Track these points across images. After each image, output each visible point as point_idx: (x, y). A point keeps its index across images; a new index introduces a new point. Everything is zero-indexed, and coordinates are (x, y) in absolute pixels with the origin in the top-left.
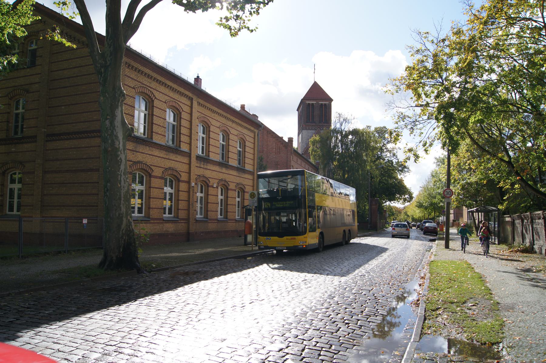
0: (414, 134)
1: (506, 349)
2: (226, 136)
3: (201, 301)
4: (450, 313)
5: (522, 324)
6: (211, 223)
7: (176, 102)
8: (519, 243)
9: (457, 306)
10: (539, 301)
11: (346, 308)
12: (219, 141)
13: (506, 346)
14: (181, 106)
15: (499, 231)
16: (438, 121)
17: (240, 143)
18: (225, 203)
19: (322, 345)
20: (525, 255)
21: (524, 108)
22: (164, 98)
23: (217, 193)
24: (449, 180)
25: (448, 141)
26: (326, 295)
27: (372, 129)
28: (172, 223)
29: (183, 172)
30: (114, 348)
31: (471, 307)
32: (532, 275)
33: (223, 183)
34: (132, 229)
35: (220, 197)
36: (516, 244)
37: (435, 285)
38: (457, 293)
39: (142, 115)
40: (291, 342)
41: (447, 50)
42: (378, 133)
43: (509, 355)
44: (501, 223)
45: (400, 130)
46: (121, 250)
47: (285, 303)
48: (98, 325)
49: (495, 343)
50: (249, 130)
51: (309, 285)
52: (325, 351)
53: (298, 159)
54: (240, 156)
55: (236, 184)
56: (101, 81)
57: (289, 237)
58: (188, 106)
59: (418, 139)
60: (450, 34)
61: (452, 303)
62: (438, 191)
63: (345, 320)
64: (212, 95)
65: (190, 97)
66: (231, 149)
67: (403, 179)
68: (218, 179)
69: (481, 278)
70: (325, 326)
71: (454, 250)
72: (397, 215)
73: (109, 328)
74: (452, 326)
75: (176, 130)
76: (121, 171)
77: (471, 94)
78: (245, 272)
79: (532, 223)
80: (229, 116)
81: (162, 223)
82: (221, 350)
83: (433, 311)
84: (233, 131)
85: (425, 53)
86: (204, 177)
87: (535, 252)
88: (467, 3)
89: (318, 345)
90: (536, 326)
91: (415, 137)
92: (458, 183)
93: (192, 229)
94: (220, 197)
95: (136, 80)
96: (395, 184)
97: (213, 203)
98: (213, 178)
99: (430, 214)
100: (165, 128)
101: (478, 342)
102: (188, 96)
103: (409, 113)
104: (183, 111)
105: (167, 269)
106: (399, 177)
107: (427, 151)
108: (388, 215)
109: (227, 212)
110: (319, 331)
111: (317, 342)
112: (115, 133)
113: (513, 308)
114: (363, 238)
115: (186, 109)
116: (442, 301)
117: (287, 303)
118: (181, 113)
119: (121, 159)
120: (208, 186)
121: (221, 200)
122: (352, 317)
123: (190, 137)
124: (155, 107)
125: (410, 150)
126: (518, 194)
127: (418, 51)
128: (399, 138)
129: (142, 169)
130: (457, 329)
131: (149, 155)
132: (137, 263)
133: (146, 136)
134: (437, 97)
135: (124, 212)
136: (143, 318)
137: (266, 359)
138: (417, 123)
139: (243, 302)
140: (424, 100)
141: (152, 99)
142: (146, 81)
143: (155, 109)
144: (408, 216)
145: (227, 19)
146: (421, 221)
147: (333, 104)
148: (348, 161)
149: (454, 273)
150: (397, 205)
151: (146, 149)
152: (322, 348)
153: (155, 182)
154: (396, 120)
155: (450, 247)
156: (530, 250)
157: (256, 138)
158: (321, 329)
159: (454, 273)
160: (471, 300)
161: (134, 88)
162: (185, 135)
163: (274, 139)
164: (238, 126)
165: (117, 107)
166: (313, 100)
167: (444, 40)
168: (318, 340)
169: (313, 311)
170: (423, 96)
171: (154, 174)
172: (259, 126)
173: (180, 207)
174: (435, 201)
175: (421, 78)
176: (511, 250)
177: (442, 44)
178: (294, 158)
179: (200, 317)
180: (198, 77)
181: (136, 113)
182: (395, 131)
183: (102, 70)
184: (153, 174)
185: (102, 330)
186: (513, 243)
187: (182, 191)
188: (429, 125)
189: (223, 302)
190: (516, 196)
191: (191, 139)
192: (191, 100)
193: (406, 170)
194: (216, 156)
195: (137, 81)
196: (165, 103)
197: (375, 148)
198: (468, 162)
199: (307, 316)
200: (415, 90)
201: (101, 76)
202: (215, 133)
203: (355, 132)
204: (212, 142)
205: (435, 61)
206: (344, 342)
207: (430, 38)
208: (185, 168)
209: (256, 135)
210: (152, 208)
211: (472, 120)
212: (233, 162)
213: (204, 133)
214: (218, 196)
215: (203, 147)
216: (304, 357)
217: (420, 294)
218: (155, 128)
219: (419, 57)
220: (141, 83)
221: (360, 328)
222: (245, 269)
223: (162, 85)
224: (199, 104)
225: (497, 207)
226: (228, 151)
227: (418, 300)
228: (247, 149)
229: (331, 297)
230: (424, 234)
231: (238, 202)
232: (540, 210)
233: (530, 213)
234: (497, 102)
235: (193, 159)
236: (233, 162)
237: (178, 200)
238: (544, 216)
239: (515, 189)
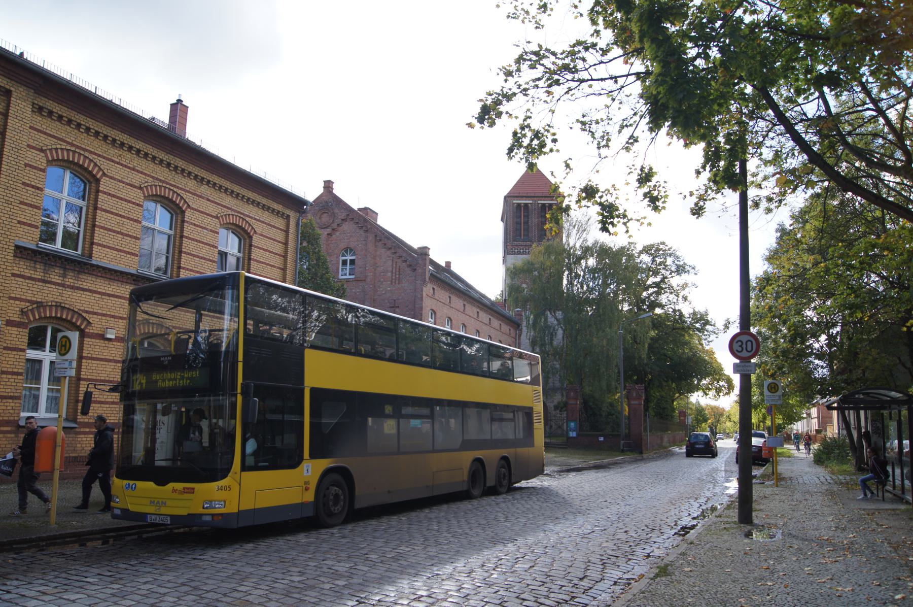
14: (185, 197)
53: (467, 305)
57: (179, 486)
64: (48, 67)
133: (79, 252)
161: (217, 217)
163: (389, 252)
166: (527, 197)
180: (179, 101)
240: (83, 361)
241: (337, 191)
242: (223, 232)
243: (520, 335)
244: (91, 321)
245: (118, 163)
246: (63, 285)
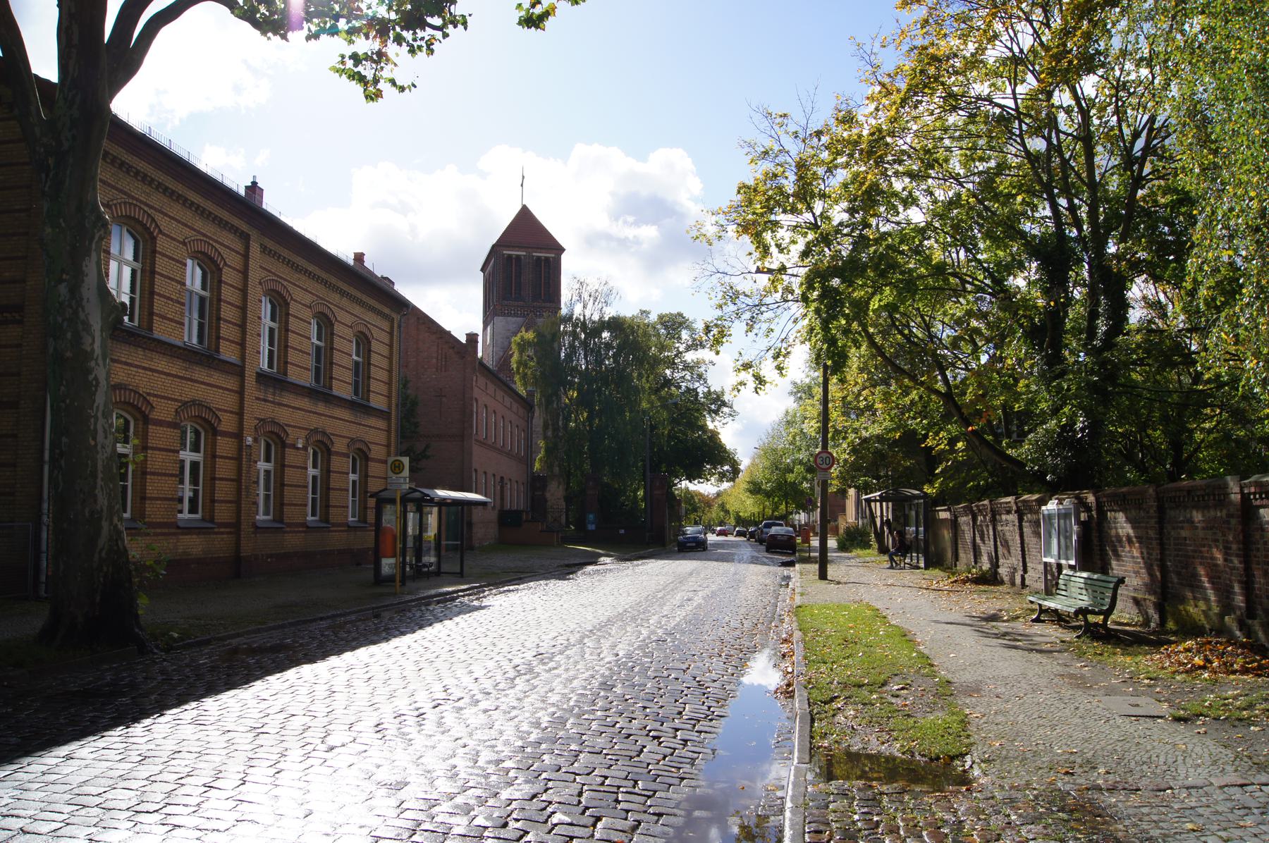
0: (755, 331)
1: (979, 764)
2: (326, 324)
3: (320, 708)
4: (860, 706)
5: (1000, 719)
6: (290, 532)
7: (209, 244)
8: (968, 565)
9: (871, 692)
10: (1024, 675)
11: (645, 708)
12: (309, 339)
13: (977, 761)
15: (926, 541)
16: (807, 303)
17: (358, 344)
18: (324, 485)
19: (617, 782)
20: (982, 588)
21: (977, 283)
23: (306, 463)
24: (824, 430)
25: (825, 346)
26: (596, 683)
27: (653, 318)
28: (198, 534)
29: (225, 411)
30: (156, 817)
31: (898, 692)
32: (1002, 627)
33: (319, 437)
34: (124, 547)
35: (311, 471)
36: (961, 566)
37: (818, 653)
38: (866, 666)
39: (127, 272)
40: (550, 780)
41: (825, 155)
42: (666, 328)
43: (986, 775)
44: (931, 523)
45: (727, 324)
46: (98, 598)
47: (511, 704)
48: (97, 772)
49: (957, 756)
50: (379, 313)
51: (552, 665)
52: (627, 792)
54: (357, 374)
56: (46, 189)
58: (238, 253)
59: (763, 343)
60: (832, 122)
61: (860, 686)
62: (797, 456)
63: (650, 731)
66: (337, 357)
67: (719, 430)
68: (306, 429)
69: (906, 636)
70: (612, 744)
71: (839, 583)
72: (703, 511)
73: (125, 777)
74: (868, 730)
75: (209, 309)
76: (98, 407)
77: (875, 252)
78: (395, 642)
79: (994, 521)
80: (333, 280)
81: (174, 534)
82: (404, 806)
83: (825, 703)
84: (342, 316)
85: (781, 159)
86: (274, 423)
87: (1002, 583)
88: (867, 58)
89: (607, 782)
90: (1027, 721)
91: (757, 339)
92: (845, 438)
93: (247, 548)
94: (311, 471)
95: (113, 187)
96: (703, 440)
97: (296, 486)
98: (295, 427)
99: (776, 508)
100: (183, 304)
101: (923, 756)
102: (237, 228)
103: (744, 285)
104: (225, 264)
105: (208, 642)
106: (710, 426)
107: (783, 368)
108: (683, 511)
109: (328, 506)
110: (602, 755)
111: (606, 778)
112: (82, 316)
113: (978, 690)
114: (640, 562)
115: (233, 260)
116: (839, 683)
117: (515, 704)
118: (220, 270)
119: (96, 379)
120: (284, 445)
121: (314, 478)
122: (662, 725)
123: (243, 326)
124: (160, 253)
125: (747, 366)
126: (963, 463)
127: (766, 153)
128: (724, 340)
129: (127, 405)
130: (879, 734)
131: (144, 368)
132: (137, 630)
133: (136, 324)
134: (805, 254)
135: (105, 508)
136: (198, 749)
137: (509, 816)
138: (763, 309)
139: (417, 705)
140: (775, 260)
141: (152, 233)
142: (137, 190)
143: (159, 259)
144: (727, 512)
145: (356, 58)
146: (756, 524)
147: (565, 258)
148: (599, 389)
149: (851, 628)
150: (706, 488)
151: (138, 356)
152: (619, 787)
153: (159, 436)
154: (718, 299)
155: (829, 578)
156: (990, 579)
158: (605, 752)
159: (851, 628)
160: (896, 679)
162: (230, 322)
164: (355, 305)
165: (88, 253)
166: (520, 247)
167: (819, 134)
168: (606, 772)
169: (579, 716)
170: (773, 250)
171: (154, 415)
172: (401, 304)
173: (218, 496)
174: (791, 477)
175: (771, 210)
176: (953, 579)
177: (815, 140)
178: (480, 381)
179: (331, 741)
180: (254, 183)
181: (113, 266)
182: (716, 325)
183: (51, 161)
184: (154, 415)
185: (111, 782)
186: (956, 566)
187: (222, 457)
188: (786, 315)
189: (372, 708)
190: (958, 466)
191: (244, 333)
194: (301, 375)
195: (117, 189)
196: (184, 243)
197: (656, 362)
198: (864, 393)
199: (568, 726)
200: (757, 237)
201: (47, 176)
202: (301, 319)
203: (616, 325)
204: (293, 340)
205: (801, 178)
206: (660, 773)
207: (792, 128)
208: (230, 401)
209: (396, 325)
211: (874, 304)
212: (343, 389)
213: (273, 319)
214: (306, 468)
215: (271, 353)
216: (587, 808)
217: (788, 673)
218: (159, 305)
219: (767, 166)
220: (125, 193)
221: (685, 745)
222: (395, 637)
223: (177, 200)
224: (264, 249)
225: (921, 490)
226: (331, 363)
227: (789, 685)
228: (375, 359)
229: (607, 686)
230: (767, 551)
231: (354, 482)
232: (1009, 496)
233: (991, 501)
234: (927, 269)
235: (250, 381)
236: (343, 389)
237: (214, 479)
238: (1018, 507)
239: (956, 452)
243: (532, 418)
246: (265, 401)
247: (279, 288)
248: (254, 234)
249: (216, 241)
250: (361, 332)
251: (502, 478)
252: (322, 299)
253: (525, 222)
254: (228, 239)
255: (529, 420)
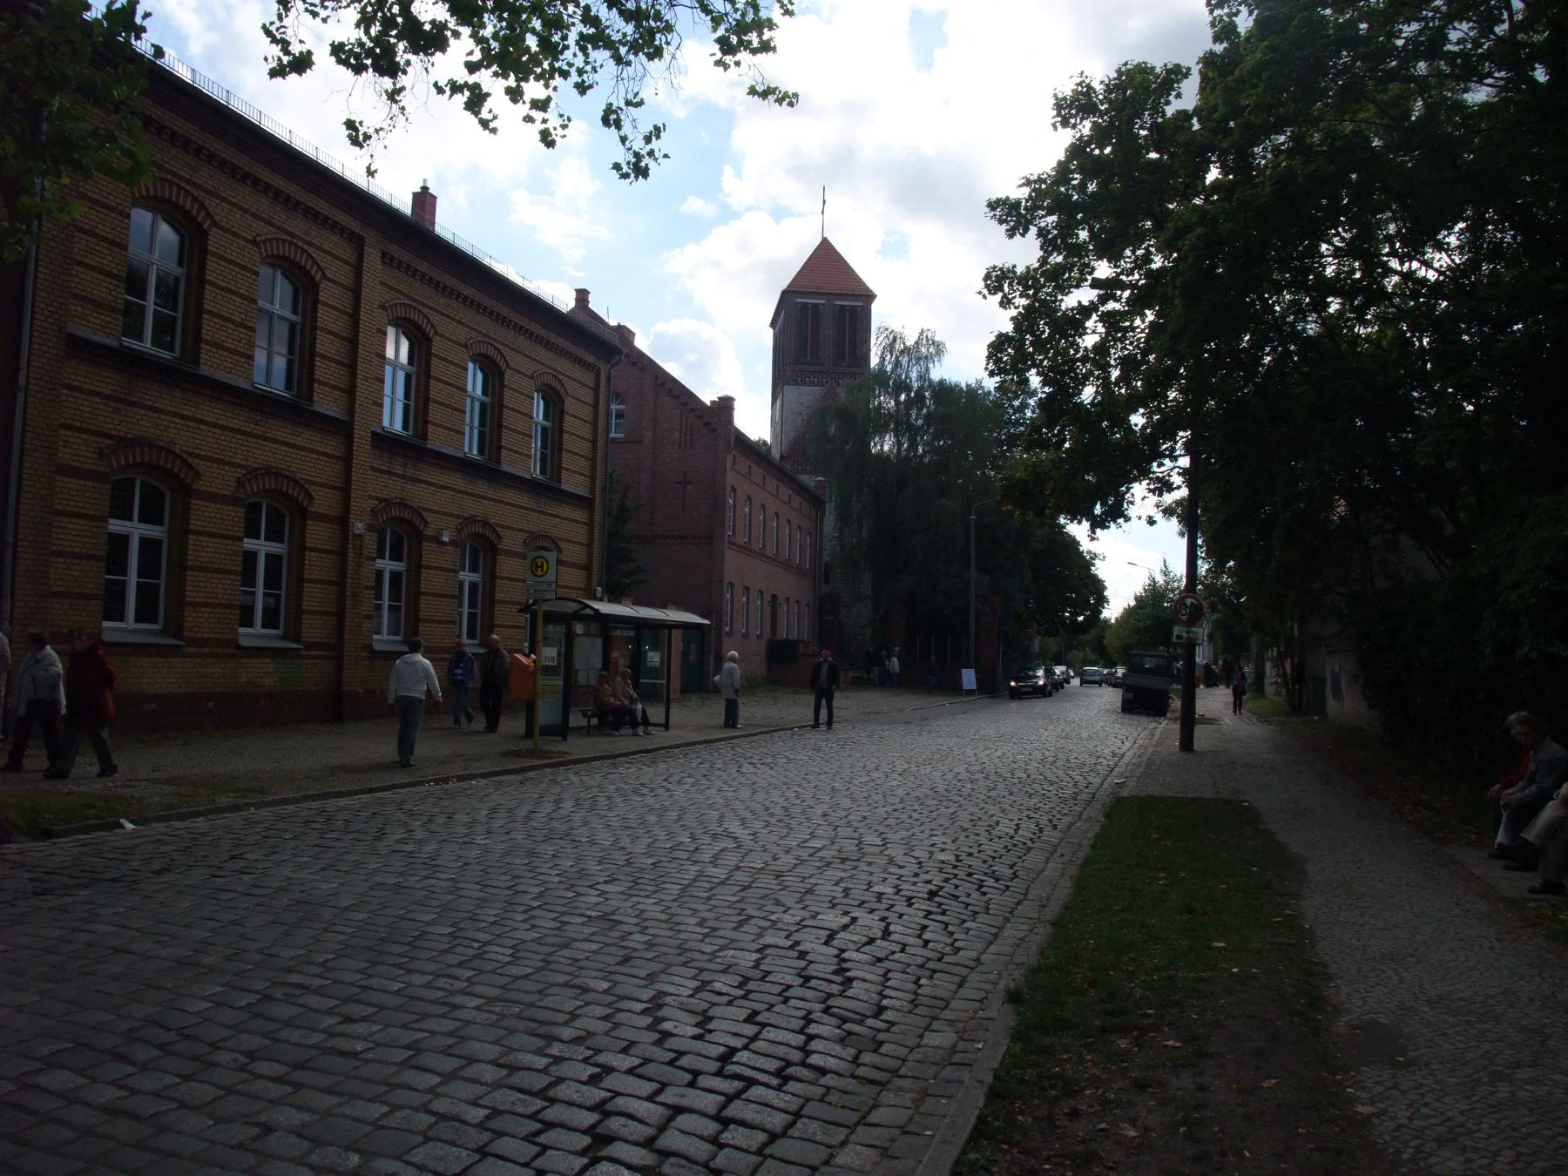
12: (254, 301)
14: (318, 259)
22: (528, 367)
29: (321, 485)
50: (579, 361)
55: (458, 521)
65: (352, 232)
68: (458, 517)
97: (438, 595)
115: (339, 272)
124: (213, 254)
131: (183, 417)
133: (410, 433)
147: (875, 307)
153: (204, 514)
157: (602, 389)
164: (538, 347)
171: (201, 485)
180: (425, 189)
187: (313, 550)
192: (358, 242)
193: (1060, 96)
196: (255, 243)
210: (194, 604)
224: (388, 260)
227: (1129, 1119)
235: (362, 444)
240: (307, 553)
241: (594, 305)
242: (266, 271)
243: (822, 519)
244: (200, 470)
245: (447, 316)
247: (416, 317)
248: (371, 239)
249: (309, 243)
250: (549, 386)
251: (774, 597)
252: (484, 335)
253: (826, 258)
254: (330, 241)
255: (819, 520)
